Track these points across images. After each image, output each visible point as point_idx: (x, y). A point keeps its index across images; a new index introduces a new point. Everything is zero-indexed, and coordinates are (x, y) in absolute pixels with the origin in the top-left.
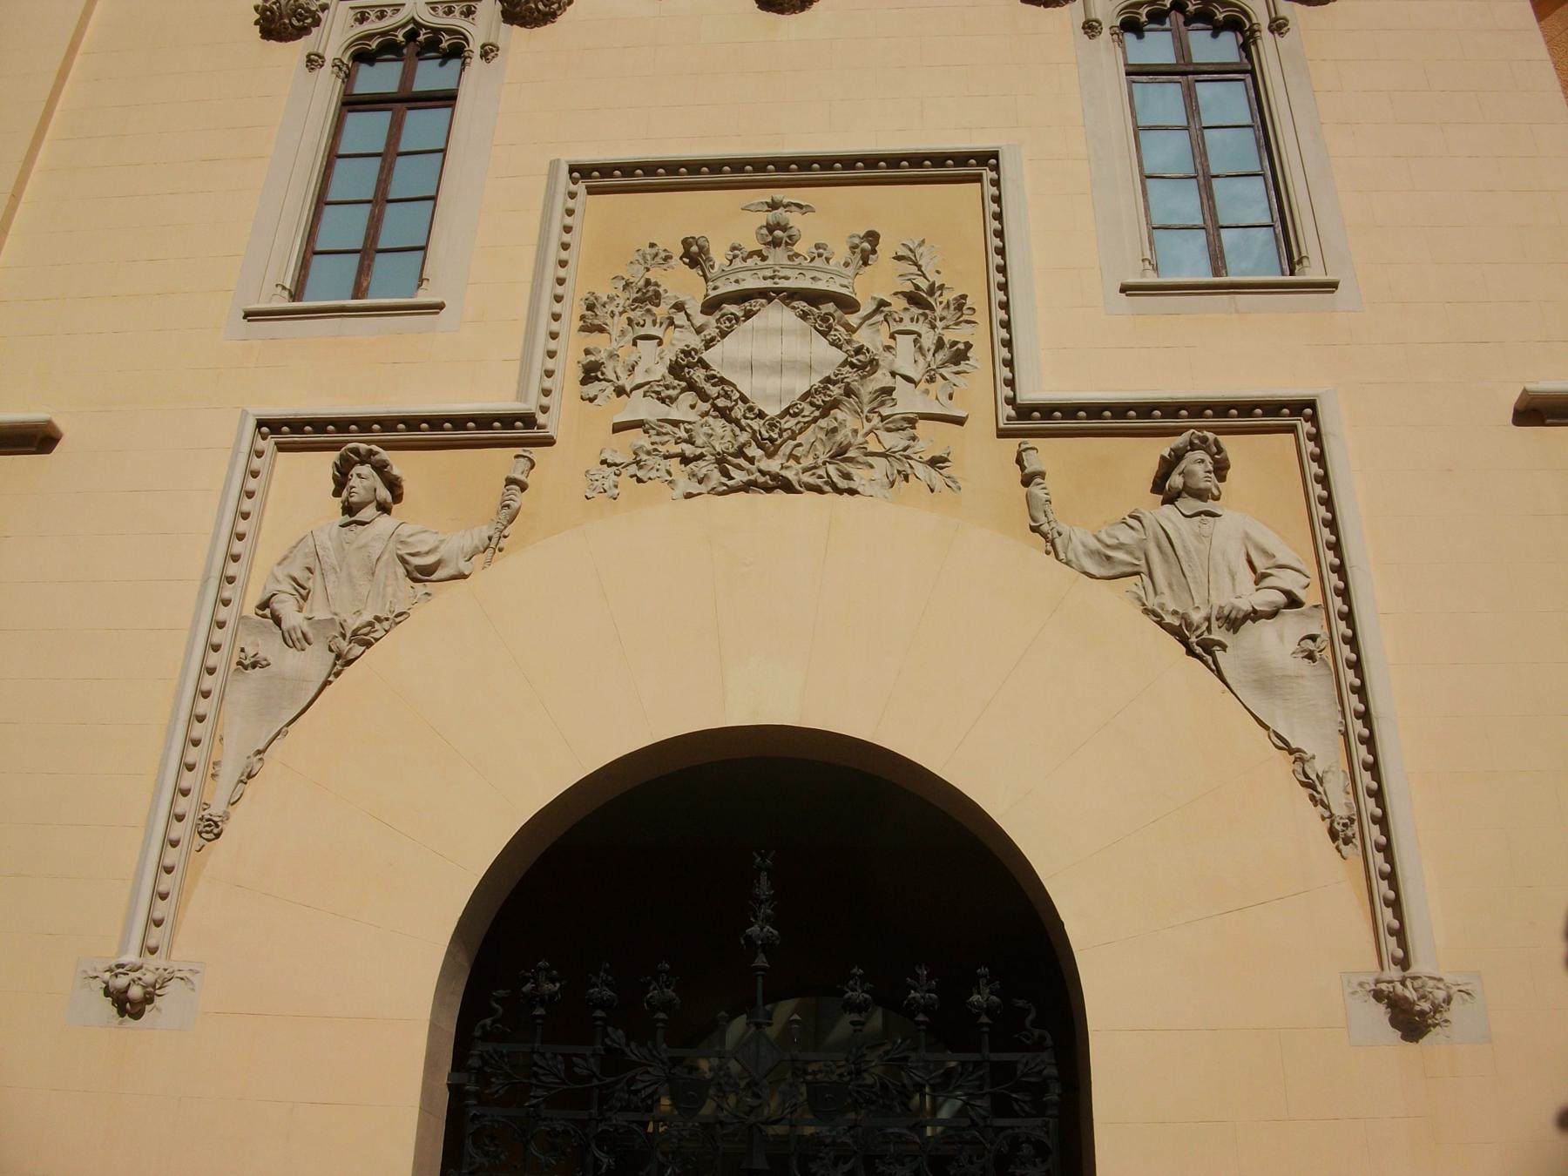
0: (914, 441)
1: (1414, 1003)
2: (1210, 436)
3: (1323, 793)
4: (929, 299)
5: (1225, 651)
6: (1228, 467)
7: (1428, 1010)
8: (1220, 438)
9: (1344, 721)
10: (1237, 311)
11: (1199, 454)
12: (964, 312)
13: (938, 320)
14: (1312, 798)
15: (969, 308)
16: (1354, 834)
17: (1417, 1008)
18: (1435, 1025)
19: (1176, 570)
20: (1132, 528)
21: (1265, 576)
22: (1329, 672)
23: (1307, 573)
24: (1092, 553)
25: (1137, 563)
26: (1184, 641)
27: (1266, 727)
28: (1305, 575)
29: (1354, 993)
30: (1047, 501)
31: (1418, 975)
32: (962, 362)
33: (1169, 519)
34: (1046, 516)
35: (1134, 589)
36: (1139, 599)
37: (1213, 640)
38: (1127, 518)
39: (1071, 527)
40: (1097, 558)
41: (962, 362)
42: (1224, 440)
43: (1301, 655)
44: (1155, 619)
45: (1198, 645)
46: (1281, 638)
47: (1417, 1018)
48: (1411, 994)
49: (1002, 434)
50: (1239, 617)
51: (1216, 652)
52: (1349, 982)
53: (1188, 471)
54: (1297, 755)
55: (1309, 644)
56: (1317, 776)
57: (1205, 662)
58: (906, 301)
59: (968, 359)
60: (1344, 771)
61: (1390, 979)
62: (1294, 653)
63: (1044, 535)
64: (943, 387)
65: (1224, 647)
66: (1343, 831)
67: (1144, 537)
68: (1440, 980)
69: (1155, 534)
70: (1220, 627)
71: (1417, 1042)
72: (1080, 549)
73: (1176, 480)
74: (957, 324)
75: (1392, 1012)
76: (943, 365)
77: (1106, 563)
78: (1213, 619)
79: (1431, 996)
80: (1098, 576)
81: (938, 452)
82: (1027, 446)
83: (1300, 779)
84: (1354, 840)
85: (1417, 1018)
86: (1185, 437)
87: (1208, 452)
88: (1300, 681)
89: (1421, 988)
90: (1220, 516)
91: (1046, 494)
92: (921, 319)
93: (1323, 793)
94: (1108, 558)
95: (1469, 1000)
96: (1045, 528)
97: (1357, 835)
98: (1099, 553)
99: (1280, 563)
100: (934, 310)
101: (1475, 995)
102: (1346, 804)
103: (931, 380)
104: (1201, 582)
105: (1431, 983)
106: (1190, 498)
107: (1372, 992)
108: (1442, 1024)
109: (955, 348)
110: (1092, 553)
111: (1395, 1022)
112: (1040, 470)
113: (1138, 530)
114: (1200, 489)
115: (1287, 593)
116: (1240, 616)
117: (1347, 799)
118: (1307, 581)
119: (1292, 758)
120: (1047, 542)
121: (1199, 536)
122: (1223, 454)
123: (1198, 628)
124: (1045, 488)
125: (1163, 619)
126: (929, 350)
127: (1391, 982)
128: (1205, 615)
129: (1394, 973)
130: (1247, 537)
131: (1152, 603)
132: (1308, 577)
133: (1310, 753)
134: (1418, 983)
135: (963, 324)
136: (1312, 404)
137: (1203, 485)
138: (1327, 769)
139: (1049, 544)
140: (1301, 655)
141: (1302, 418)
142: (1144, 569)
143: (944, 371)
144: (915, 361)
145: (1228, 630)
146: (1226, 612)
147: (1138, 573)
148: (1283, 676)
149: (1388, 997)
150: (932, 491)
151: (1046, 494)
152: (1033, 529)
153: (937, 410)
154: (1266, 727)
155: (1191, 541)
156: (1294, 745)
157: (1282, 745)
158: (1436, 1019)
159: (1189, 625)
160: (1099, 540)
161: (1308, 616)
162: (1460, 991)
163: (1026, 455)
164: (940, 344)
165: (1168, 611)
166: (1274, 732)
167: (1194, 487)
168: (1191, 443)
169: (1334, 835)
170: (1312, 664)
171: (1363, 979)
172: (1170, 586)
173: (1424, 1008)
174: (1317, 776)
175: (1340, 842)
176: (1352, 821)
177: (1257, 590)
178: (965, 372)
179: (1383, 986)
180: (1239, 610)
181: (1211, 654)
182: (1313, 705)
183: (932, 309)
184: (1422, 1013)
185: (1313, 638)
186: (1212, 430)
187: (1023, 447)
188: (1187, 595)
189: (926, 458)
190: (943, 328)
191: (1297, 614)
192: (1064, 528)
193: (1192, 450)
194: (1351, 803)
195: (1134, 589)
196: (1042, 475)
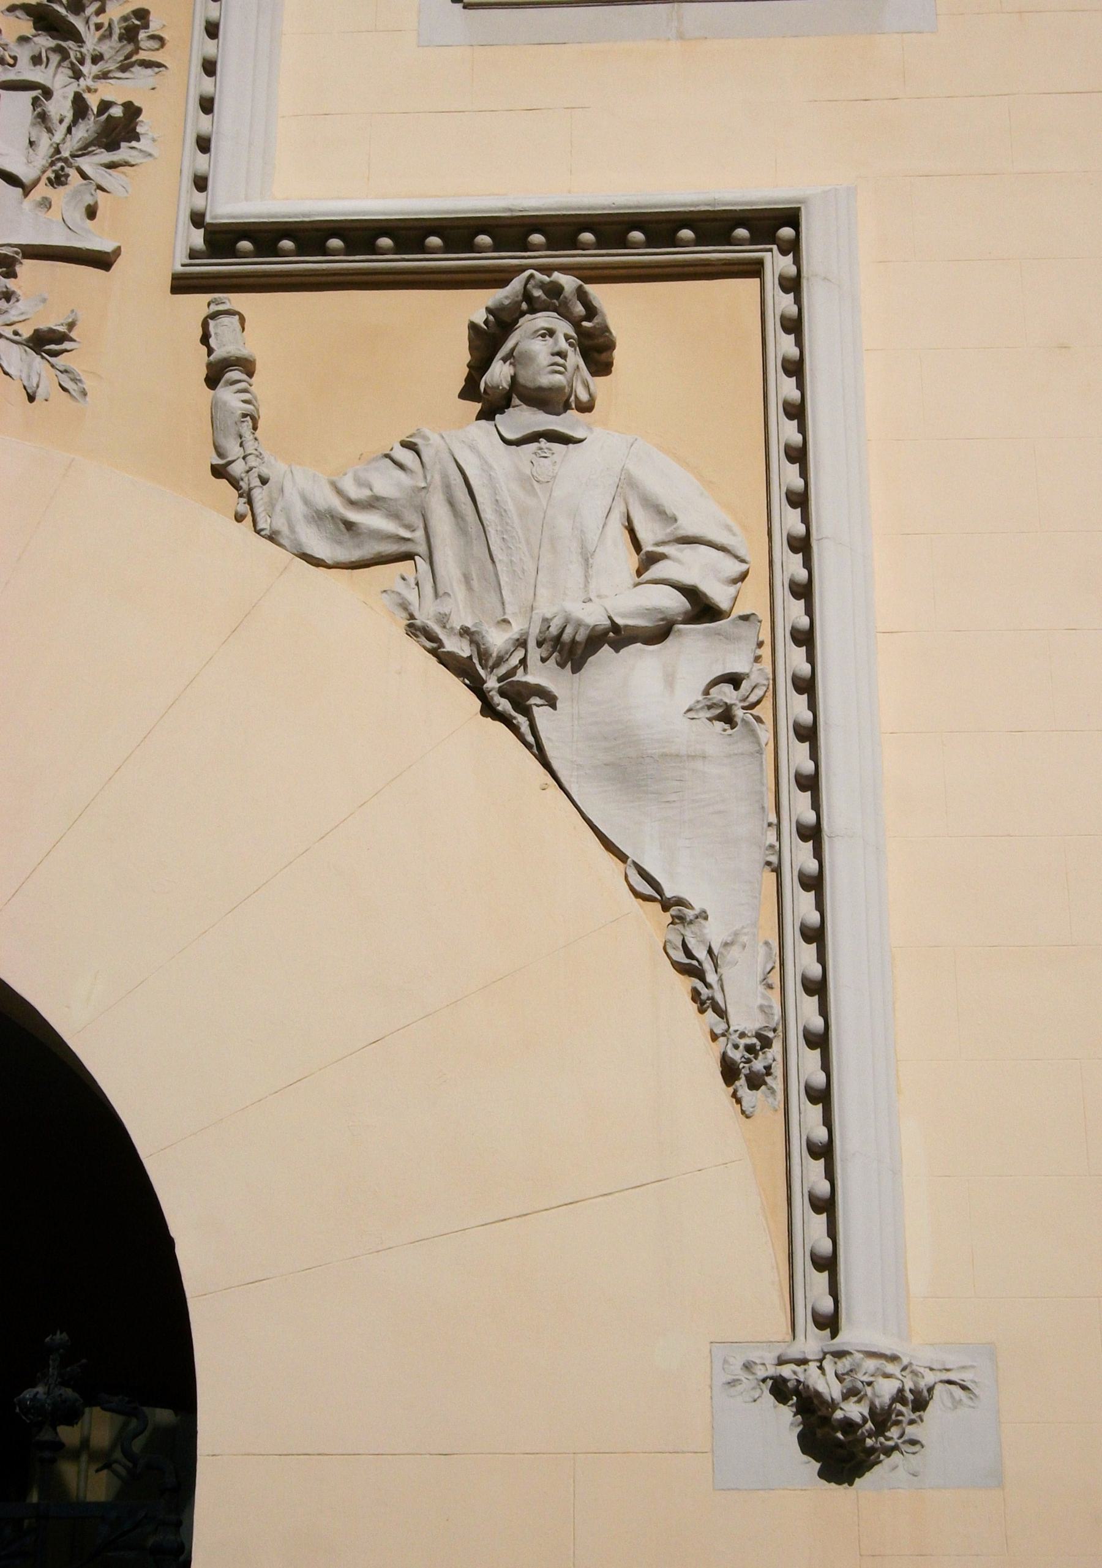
0: (8, 301)
1: (833, 1406)
2: (568, 282)
3: (716, 986)
4: (72, 18)
5: (553, 706)
6: (610, 346)
7: (858, 1419)
8: (592, 289)
9: (777, 844)
10: (681, 37)
11: (544, 320)
12: (143, 44)
13: (88, 61)
14: (696, 995)
15: (153, 37)
16: (768, 1068)
17: (838, 1415)
18: (889, 1451)
19: (480, 550)
20: (401, 466)
21: (651, 559)
22: (754, 748)
23: (742, 553)
24: (321, 517)
25: (406, 534)
26: (477, 687)
27: (622, 857)
28: (737, 557)
29: (732, 1383)
30: (245, 415)
31: (846, 1349)
32: (123, 144)
33: (473, 448)
34: (241, 445)
35: (400, 586)
36: (404, 606)
37: (526, 684)
38: (397, 447)
39: (290, 466)
40: (331, 526)
41: (123, 144)
42: (597, 292)
43: (709, 714)
44: (429, 645)
45: (502, 693)
46: (670, 680)
47: (840, 1435)
48: (827, 1386)
49: (182, 285)
50: (578, 638)
51: (535, 708)
52: (725, 1361)
53: (521, 354)
54: (674, 910)
55: (726, 694)
56: (710, 951)
57: (515, 729)
58: (31, 24)
59: (137, 137)
60: (767, 943)
61: (799, 1356)
62: (690, 710)
63: (235, 483)
64: (77, 193)
65: (551, 701)
66: (748, 1061)
67: (423, 485)
68: (894, 1358)
69: (445, 477)
70: (543, 660)
71: (851, 1484)
72: (299, 509)
73: (499, 373)
74: (124, 68)
75: (803, 1423)
76: (84, 150)
77: (346, 537)
78: (532, 644)
79: (869, 1390)
80: (329, 562)
81: (54, 322)
82: (221, 308)
83: (675, 958)
84: (768, 1079)
85: (840, 1435)
86: (516, 284)
87: (564, 312)
88: (699, 765)
89: (847, 1374)
90: (580, 441)
91: (245, 402)
92: (55, 58)
93: (716, 986)
94: (349, 526)
95: (965, 1400)
96: (237, 469)
97: (777, 1070)
98: (332, 517)
99: (682, 533)
100: (83, 42)
101: (976, 1391)
102: (762, 1008)
103: (59, 180)
104: (523, 571)
105: (871, 1364)
106: (524, 406)
107: (770, 1382)
108: (904, 1448)
109: (105, 116)
110: (321, 517)
111: (809, 1443)
112: (238, 354)
113: (412, 471)
114: (540, 389)
115: (691, 593)
116: (581, 637)
117: (764, 997)
118: (738, 568)
119: (667, 917)
120: (241, 496)
121: (528, 482)
122: (596, 320)
123: (500, 660)
124: (245, 391)
125: (441, 644)
126: (61, 121)
127: (803, 1362)
128: (517, 636)
129: (812, 1342)
130: (627, 483)
131: (425, 617)
132: (743, 561)
133: (698, 905)
134: (844, 1364)
135: (136, 69)
136: (791, 217)
137: (547, 380)
138: (729, 940)
139: (244, 500)
140: (709, 714)
141: (775, 247)
142: (422, 549)
143: (85, 163)
144: (31, 143)
145: (561, 665)
146: (554, 630)
147: (409, 556)
148: (664, 756)
149: (796, 1392)
150: (31, 398)
151: (245, 402)
152: (219, 472)
153: (58, 238)
154: (622, 857)
155: (510, 492)
156: (669, 893)
157: (648, 890)
158: (888, 1439)
159: (483, 655)
160: (339, 492)
161: (728, 638)
162: (950, 1382)
163: (216, 326)
164: (80, 108)
165: (452, 628)
166: (635, 863)
167: (530, 385)
168: (527, 296)
169: (729, 1072)
170: (730, 732)
171: (754, 1356)
172: (467, 579)
173: (848, 1415)
174: (710, 951)
175: (742, 1082)
176: (766, 1043)
177: (636, 585)
178: (127, 164)
179: (786, 1371)
180: (579, 624)
181: (527, 712)
182: (720, 812)
183: (78, 39)
184: (849, 1425)
185: (734, 680)
186: (577, 273)
187: (214, 308)
188: (494, 598)
189: (26, 332)
190: (97, 77)
191: (707, 634)
192: (275, 468)
193: (533, 310)
194: (771, 1007)
195: (400, 586)
196: (247, 366)
